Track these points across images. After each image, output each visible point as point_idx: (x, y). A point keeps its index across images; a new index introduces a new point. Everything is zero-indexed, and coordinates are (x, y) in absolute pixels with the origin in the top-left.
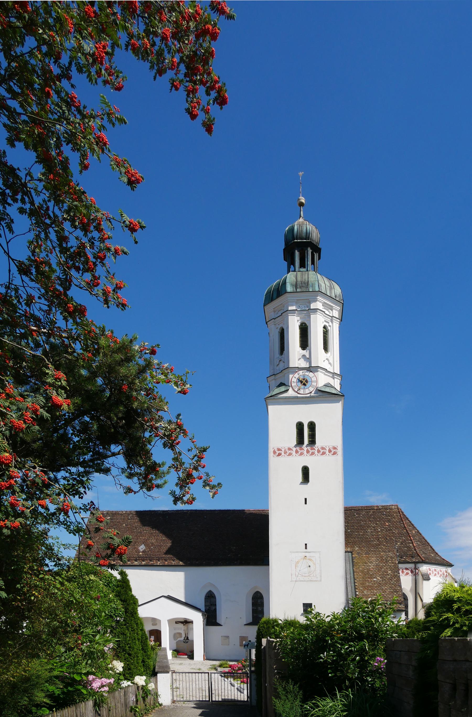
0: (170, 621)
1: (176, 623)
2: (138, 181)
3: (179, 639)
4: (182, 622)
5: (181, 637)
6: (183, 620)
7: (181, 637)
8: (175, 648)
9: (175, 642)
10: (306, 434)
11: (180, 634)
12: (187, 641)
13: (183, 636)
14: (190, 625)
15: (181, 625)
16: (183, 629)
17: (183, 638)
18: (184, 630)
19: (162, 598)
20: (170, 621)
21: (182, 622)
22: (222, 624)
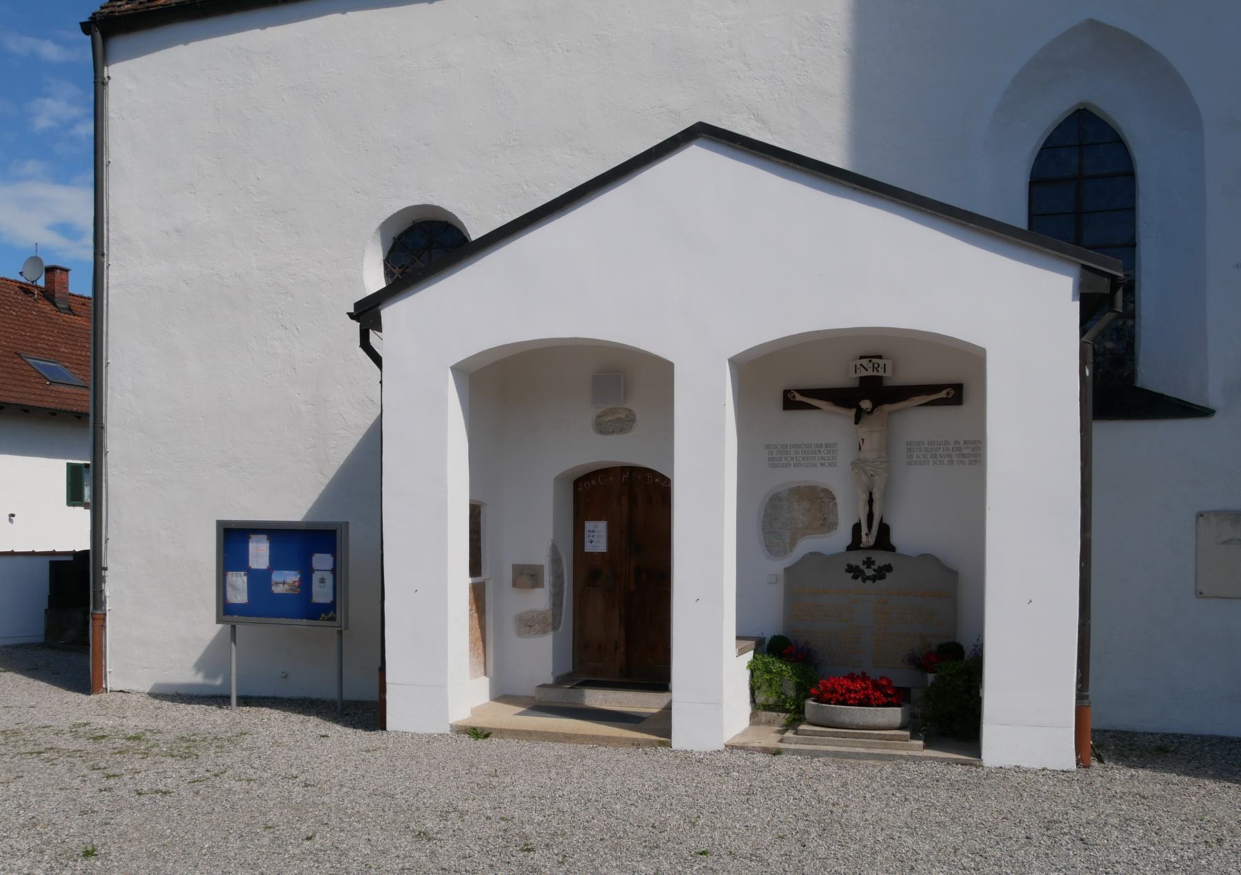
0: (751, 371)
1: (790, 402)
2: (11, 521)
3: (807, 545)
4: (841, 397)
5: (827, 525)
6: (841, 376)
7: (827, 525)
8: (771, 626)
9: (778, 566)
10: (322, 581)
11: (818, 501)
12: (881, 558)
13: (848, 513)
14: (920, 424)
15: (831, 425)
16: (845, 456)
17: (841, 537)
18: (858, 465)
19: (695, 153)
20: (751, 371)
21: (841, 397)
22: (1213, 399)
